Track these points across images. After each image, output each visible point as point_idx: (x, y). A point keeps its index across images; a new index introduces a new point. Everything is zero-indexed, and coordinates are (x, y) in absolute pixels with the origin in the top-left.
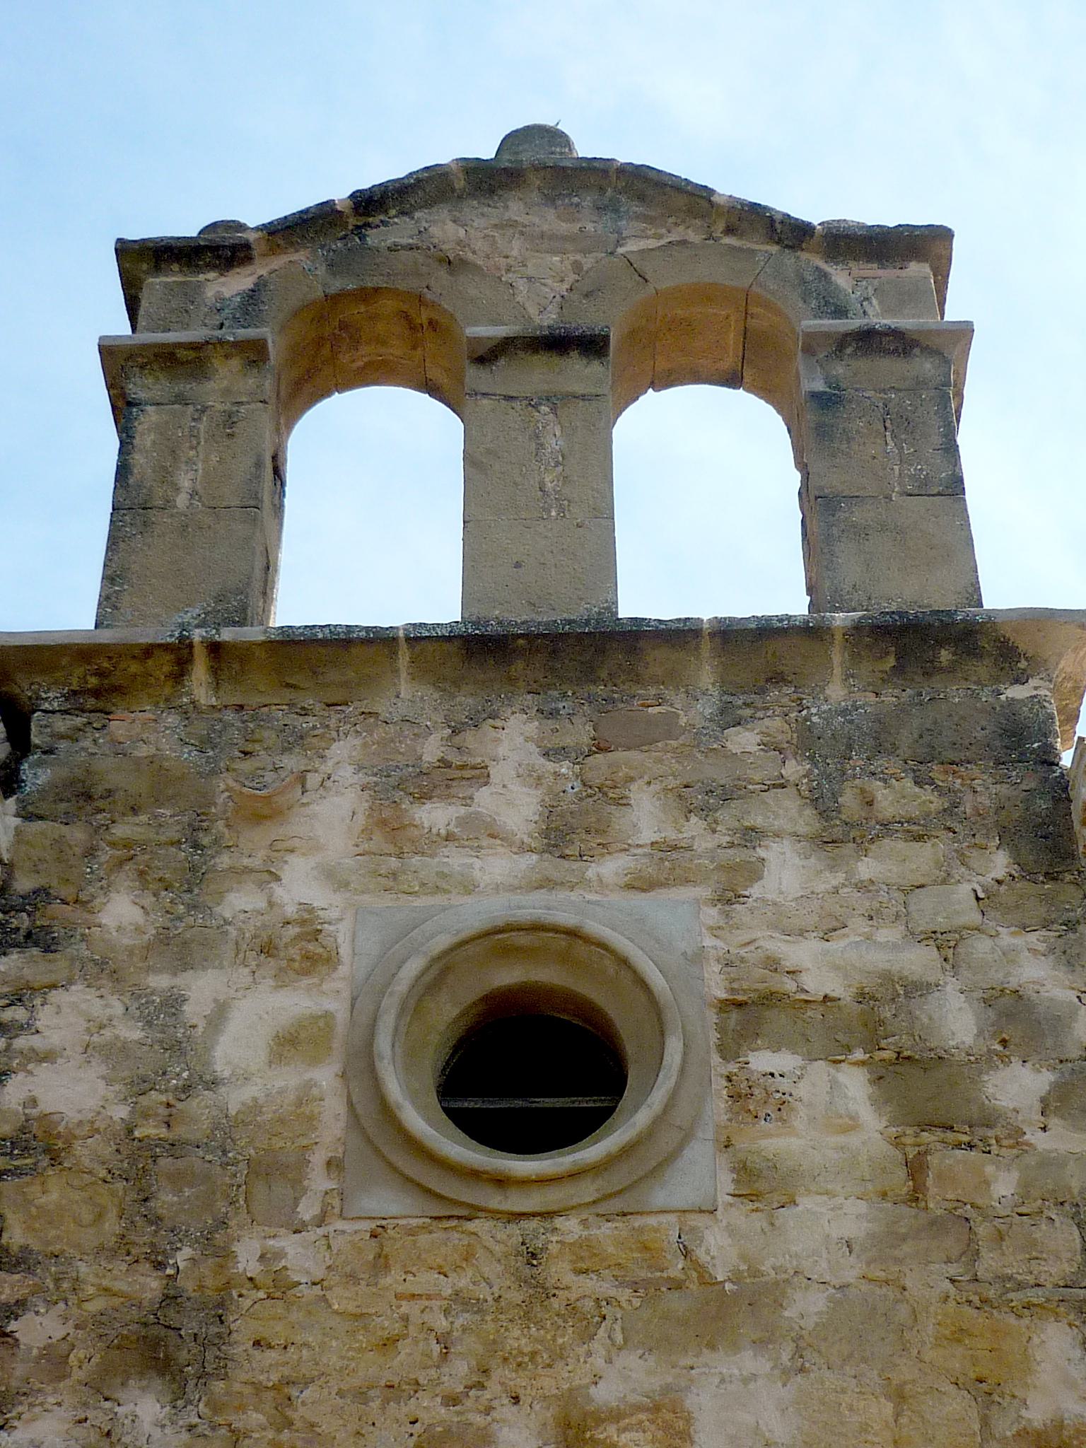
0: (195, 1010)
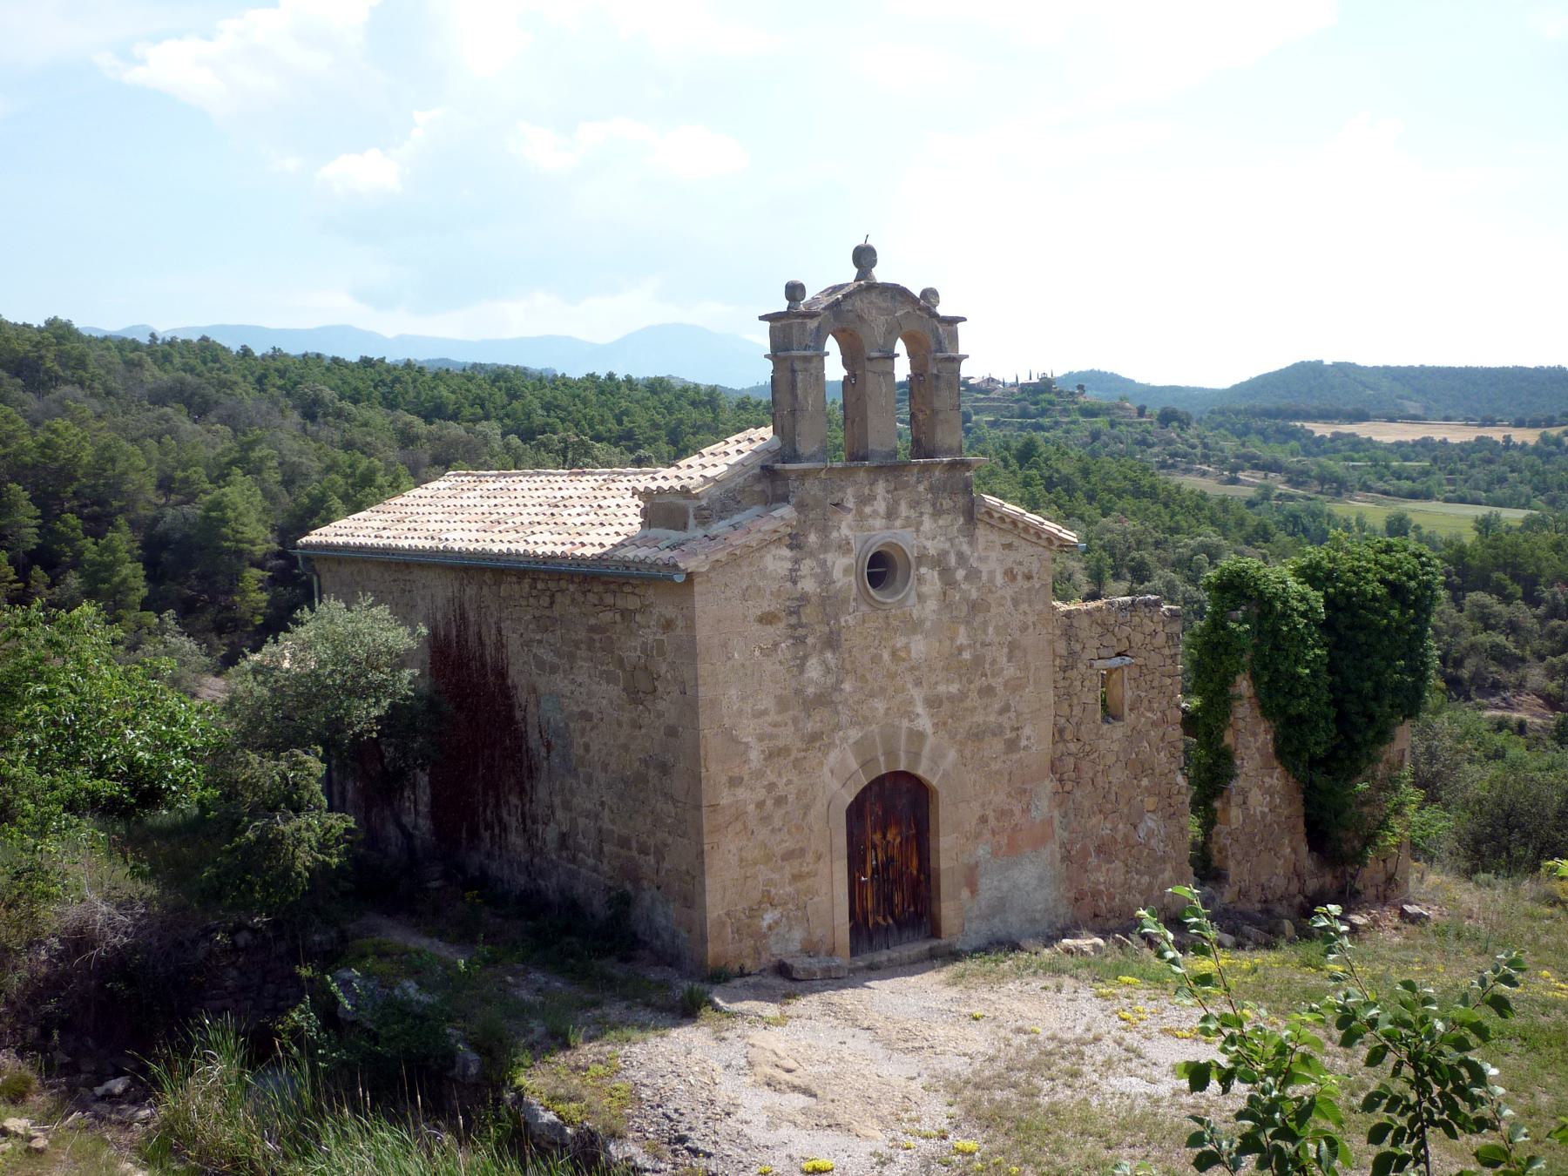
0: (829, 564)
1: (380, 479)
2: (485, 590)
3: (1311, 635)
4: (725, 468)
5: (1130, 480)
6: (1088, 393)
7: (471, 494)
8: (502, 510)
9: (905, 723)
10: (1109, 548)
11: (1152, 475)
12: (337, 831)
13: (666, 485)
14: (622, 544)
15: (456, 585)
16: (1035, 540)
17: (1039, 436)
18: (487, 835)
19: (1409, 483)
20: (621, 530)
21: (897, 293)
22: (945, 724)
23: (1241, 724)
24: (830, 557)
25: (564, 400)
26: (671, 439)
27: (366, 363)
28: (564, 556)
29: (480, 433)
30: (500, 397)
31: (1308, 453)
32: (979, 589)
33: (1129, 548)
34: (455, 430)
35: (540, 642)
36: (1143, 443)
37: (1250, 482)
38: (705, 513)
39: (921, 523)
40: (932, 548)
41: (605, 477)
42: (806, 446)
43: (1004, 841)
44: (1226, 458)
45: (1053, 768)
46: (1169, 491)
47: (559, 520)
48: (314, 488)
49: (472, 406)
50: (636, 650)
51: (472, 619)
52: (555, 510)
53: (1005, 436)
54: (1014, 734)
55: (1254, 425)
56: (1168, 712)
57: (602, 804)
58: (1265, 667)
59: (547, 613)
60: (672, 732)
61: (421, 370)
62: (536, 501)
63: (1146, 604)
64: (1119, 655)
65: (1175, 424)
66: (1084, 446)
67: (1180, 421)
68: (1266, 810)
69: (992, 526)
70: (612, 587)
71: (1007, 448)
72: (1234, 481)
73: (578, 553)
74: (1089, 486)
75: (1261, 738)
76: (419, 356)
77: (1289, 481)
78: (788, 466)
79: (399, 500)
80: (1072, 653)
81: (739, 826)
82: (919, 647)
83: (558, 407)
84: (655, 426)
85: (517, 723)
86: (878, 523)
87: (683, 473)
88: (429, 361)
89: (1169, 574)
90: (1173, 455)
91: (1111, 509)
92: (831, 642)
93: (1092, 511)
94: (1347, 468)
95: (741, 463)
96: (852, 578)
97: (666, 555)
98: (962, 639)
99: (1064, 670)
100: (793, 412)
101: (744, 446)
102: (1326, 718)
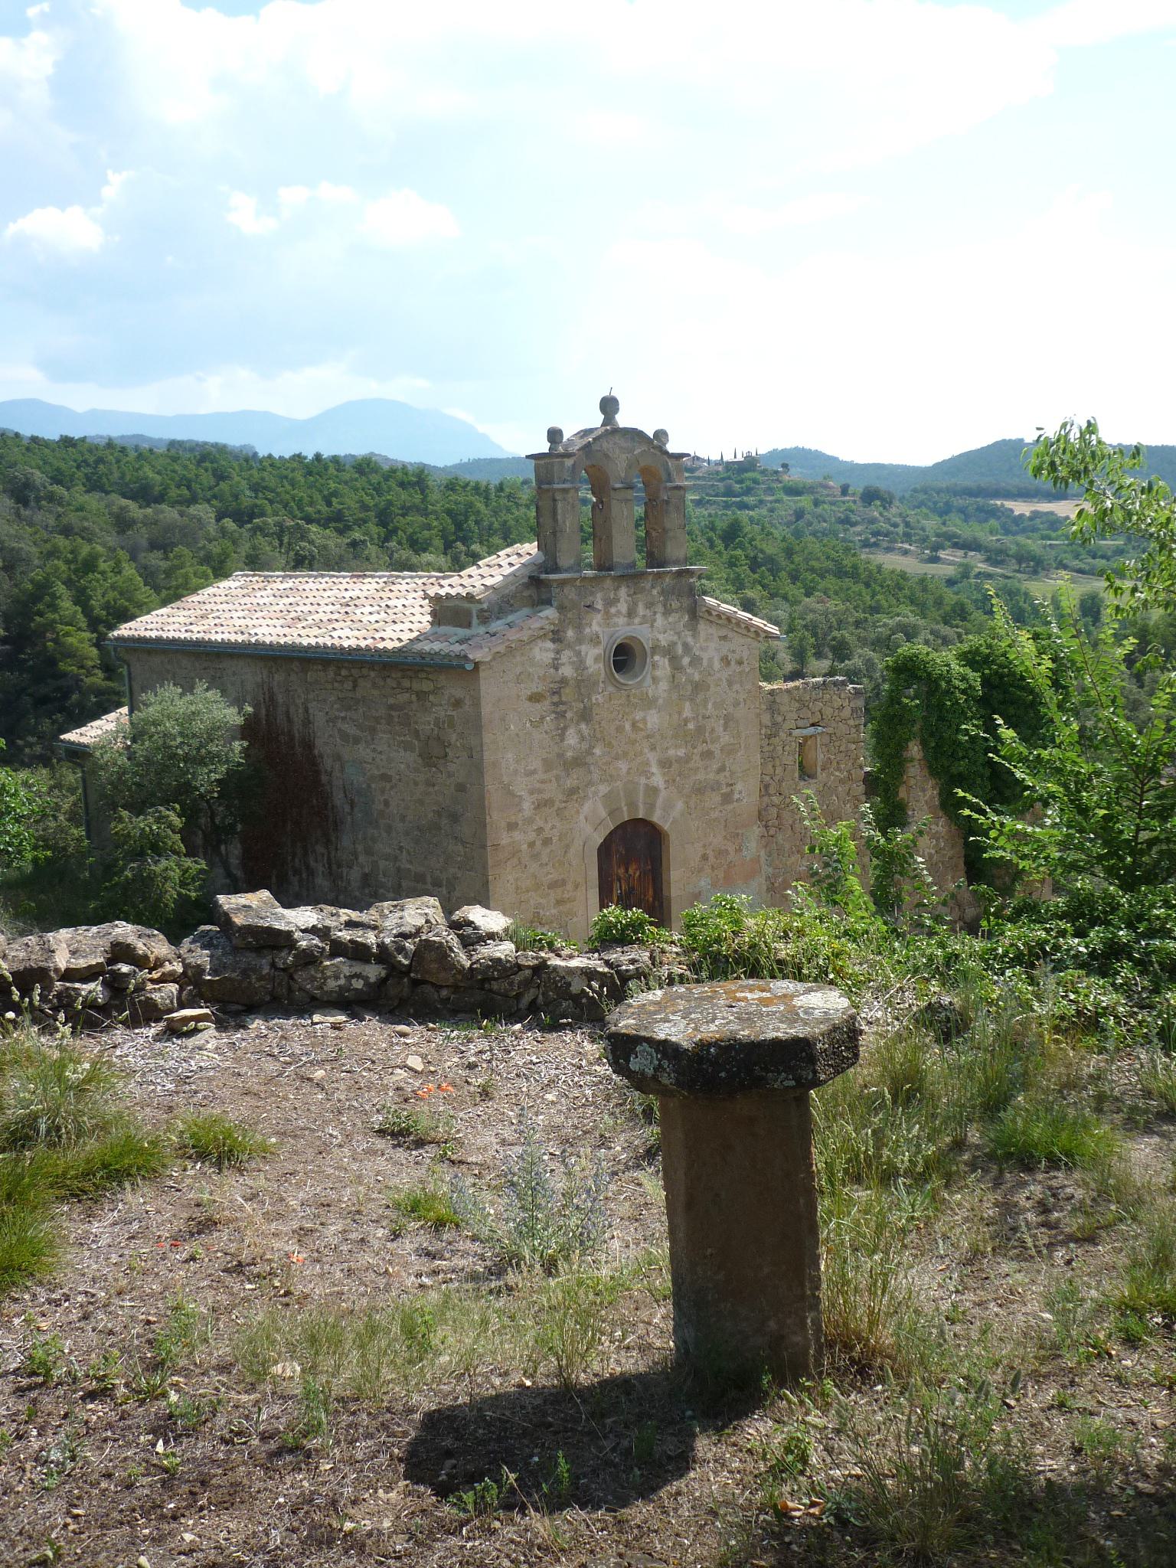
1: (103, 566)
2: (293, 677)
3: (970, 708)
4: (501, 578)
5: (833, 560)
6: (792, 471)
7: (263, 593)
8: (298, 609)
9: (643, 781)
10: (812, 628)
11: (854, 555)
12: (193, 872)
13: (453, 592)
14: (417, 639)
15: (265, 672)
16: (745, 632)
17: (744, 515)
18: (295, 880)
19: (1104, 561)
20: (414, 627)
21: (636, 434)
22: (674, 781)
23: (912, 782)
24: (583, 648)
25: (272, 481)
26: (380, 520)
27: (67, 442)
28: (368, 649)
29: (194, 517)
30: (207, 479)
31: (1007, 532)
32: (700, 673)
33: (830, 627)
34: (169, 513)
35: (344, 719)
36: (846, 521)
37: (951, 558)
38: (486, 614)
39: (655, 620)
40: (664, 640)
41: (385, 579)
42: (565, 561)
43: (721, 875)
44: (928, 537)
45: (760, 817)
46: (870, 572)
47: (355, 618)
48: (37, 575)
49: (178, 487)
50: (429, 724)
51: (281, 701)
52: (348, 609)
53: (710, 515)
54: (729, 789)
55: (955, 503)
56: (853, 772)
57: (401, 848)
58: (932, 735)
59: (350, 695)
60: (461, 788)
61: (123, 450)
62: (327, 601)
63: (835, 684)
64: (813, 725)
65: (878, 503)
66: (788, 524)
67: (883, 500)
68: (933, 852)
69: (711, 622)
70: (409, 673)
71: (713, 529)
72: (935, 560)
73: (381, 646)
74: (793, 566)
75: (929, 793)
76: (115, 431)
77: (988, 560)
78: (552, 576)
79: (195, 598)
80: (775, 724)
81: (515, 861)
82: (654, 719)
83: (265, 488)
84: (365, 507)
85: (323, 785)
86: (622, 620)
87: (466, 581)
88: (123, 437)
89: (868, 652)
90: (876, 534)
91: (814, 588)
92: (585, 716)
93: (795, 591)
94: (1045, 547)
95: (513, 574)
96: (601, 665)
97: (457, 648)
98: (687, 712)
99: (769, 737)
100: (554, 533)
101: (514, 559)
102: (982, 776)
